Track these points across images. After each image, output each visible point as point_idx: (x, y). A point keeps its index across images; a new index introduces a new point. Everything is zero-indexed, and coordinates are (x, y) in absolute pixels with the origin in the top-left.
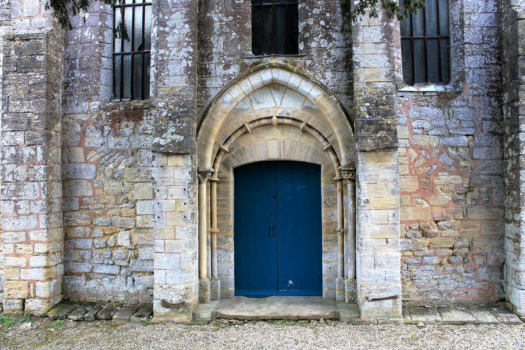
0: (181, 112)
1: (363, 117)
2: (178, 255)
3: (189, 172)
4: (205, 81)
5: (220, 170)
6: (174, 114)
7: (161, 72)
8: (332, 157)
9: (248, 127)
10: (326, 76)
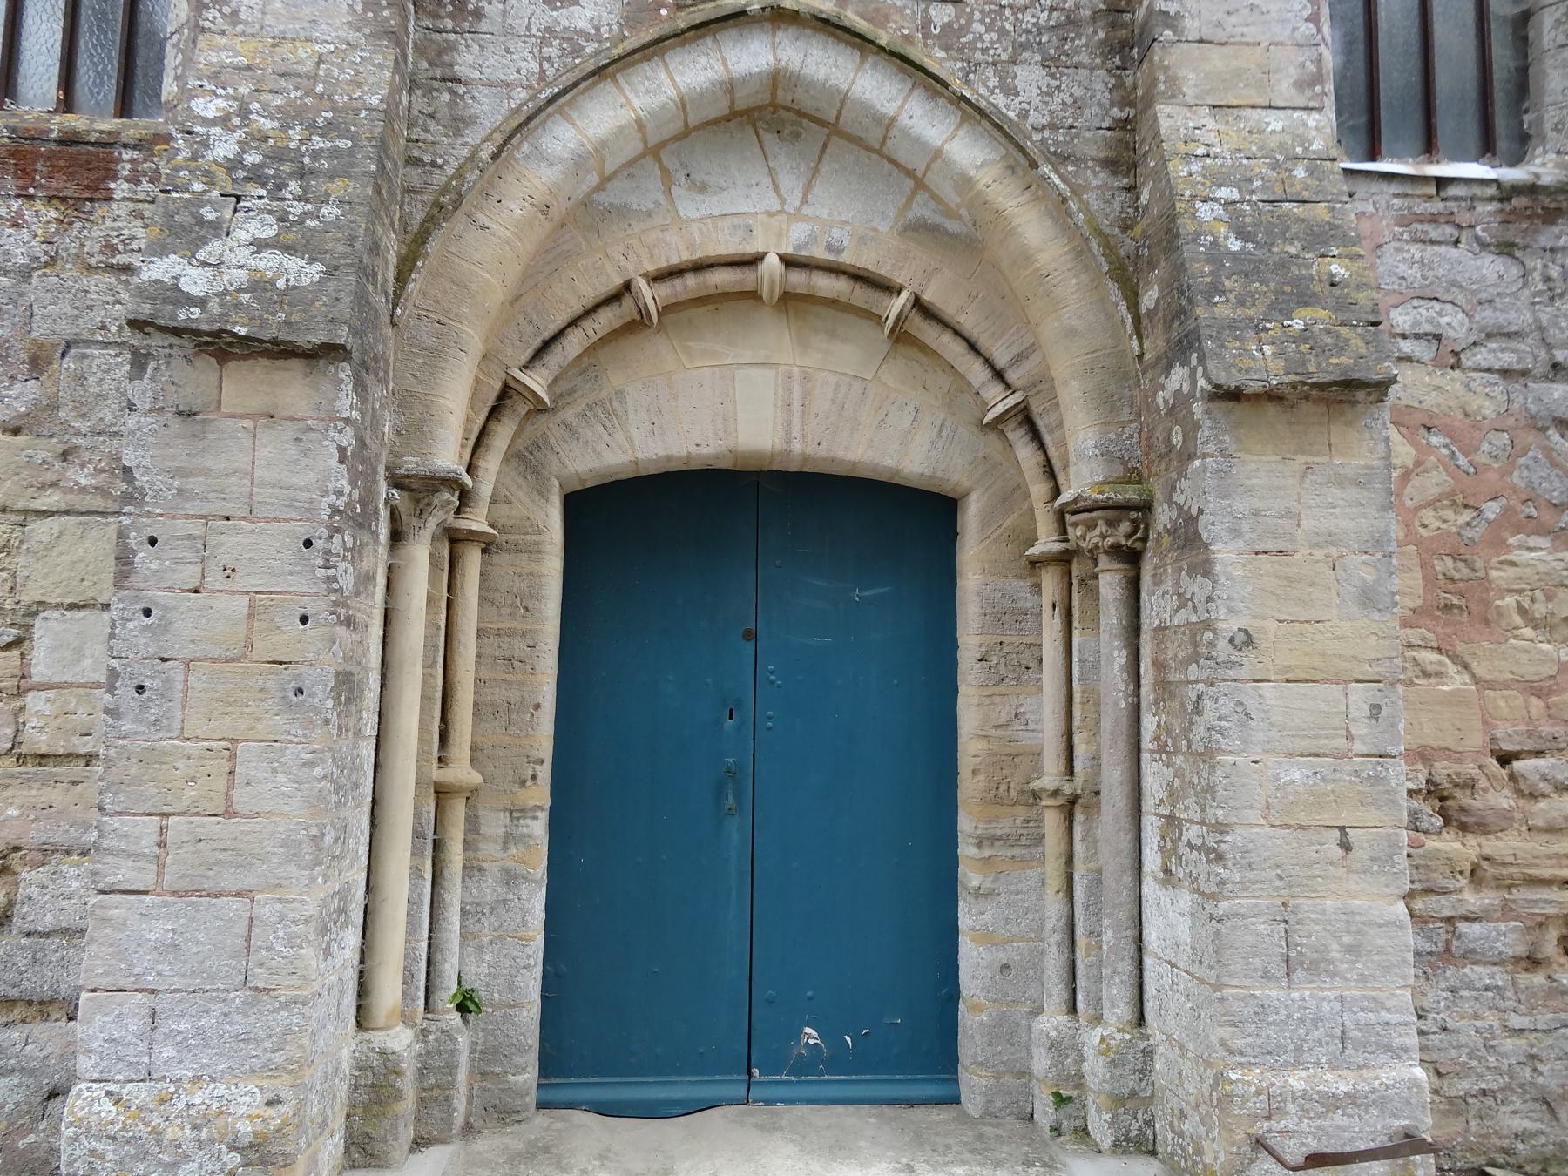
0: (316, 155)
2: (235, 904)
3: (342, 450)
4: (452, 47)
6: (277, 156)
8: (1026, 453)
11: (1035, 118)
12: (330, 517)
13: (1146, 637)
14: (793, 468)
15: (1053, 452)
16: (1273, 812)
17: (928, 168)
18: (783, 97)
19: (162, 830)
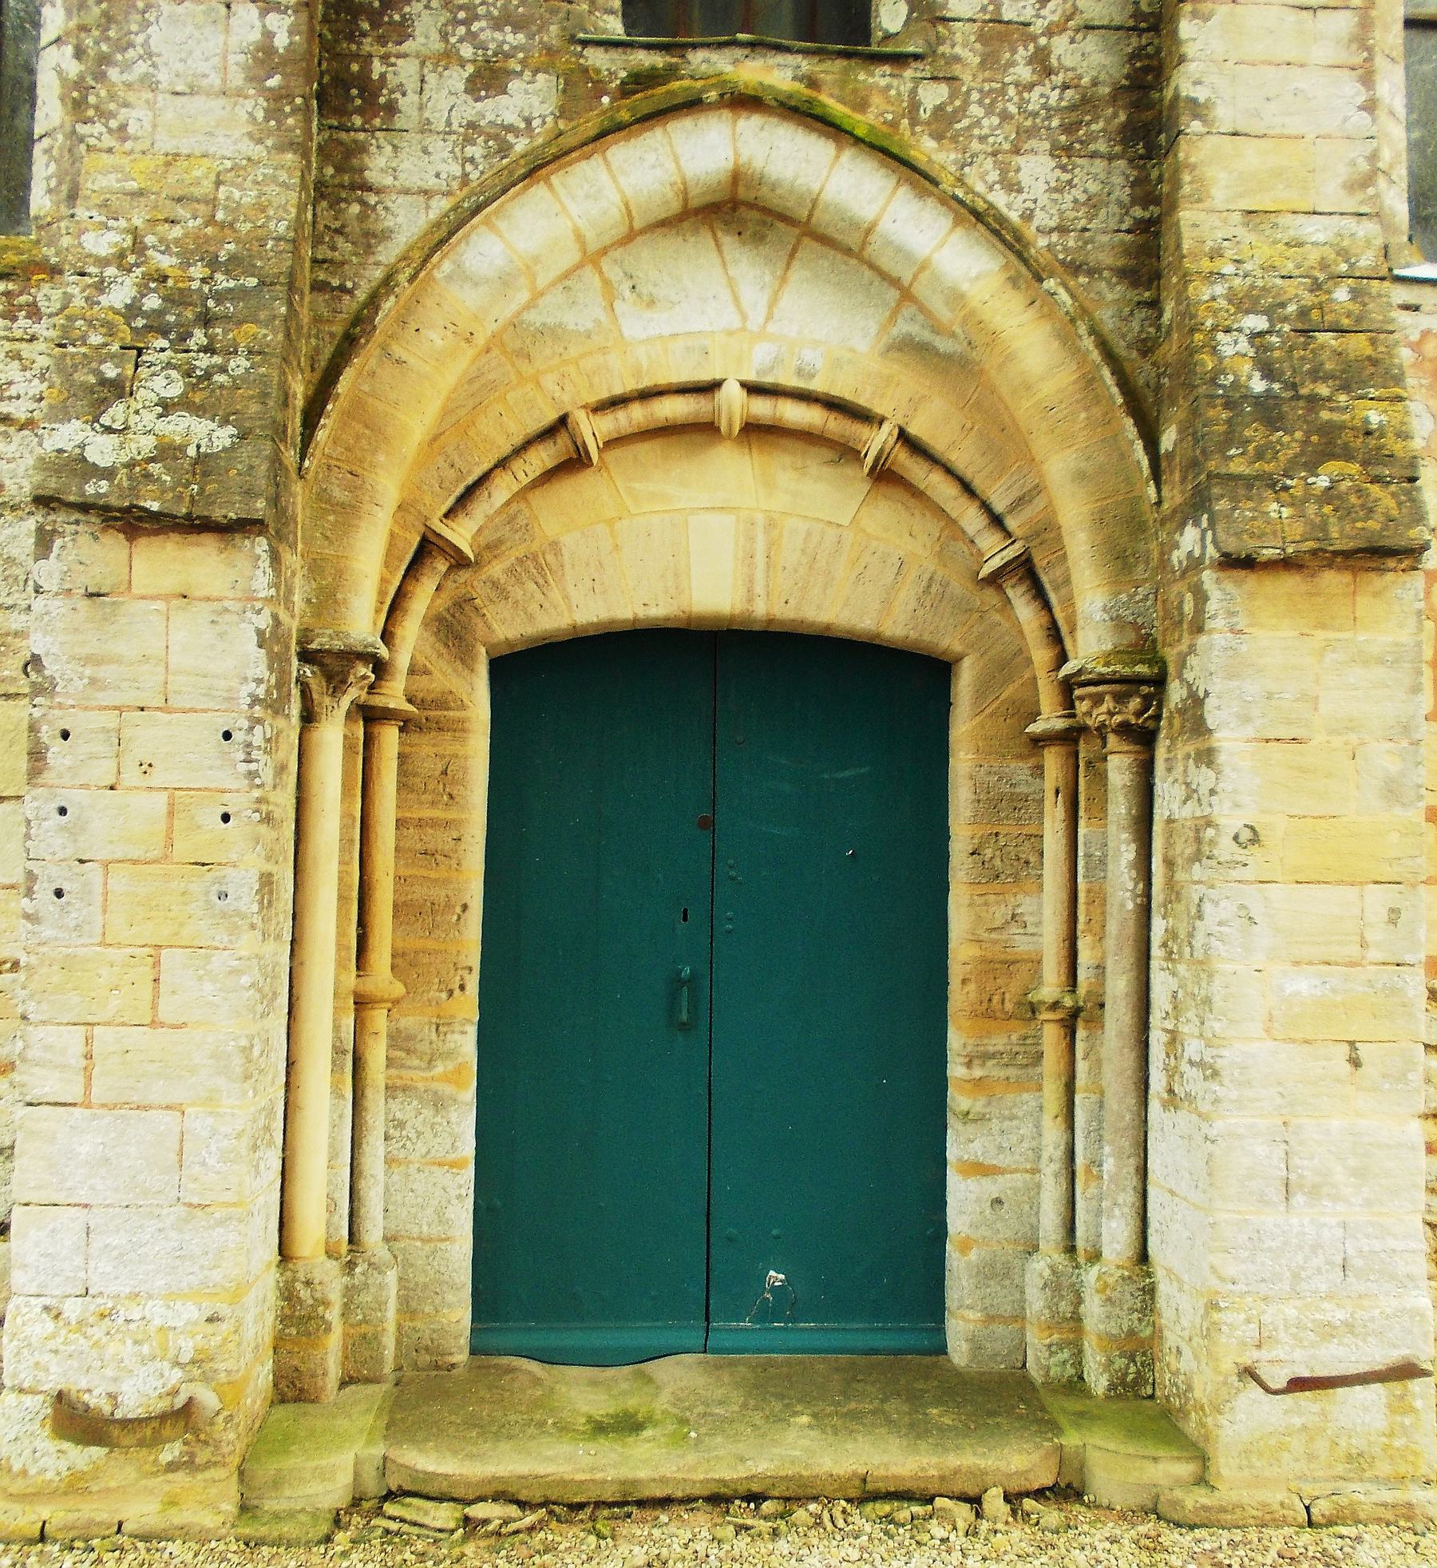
0: (220, 297)
1: (1236, 385)
3: (260, 633)
4: (362, 148)
5: (421, 660)
6: (178, 299)
7: (104, 60)
8: (1025, 612)
9: (592, 430)
10: (1024, 178)
11: (1041, 219)
12: (251, 706)
13: (1158, 828)
14: (757, 628)
15: (1059, 615)
16: (1276, 1025)
17: (915, 277)
18: (742, 193)
19: (88, 1041)
